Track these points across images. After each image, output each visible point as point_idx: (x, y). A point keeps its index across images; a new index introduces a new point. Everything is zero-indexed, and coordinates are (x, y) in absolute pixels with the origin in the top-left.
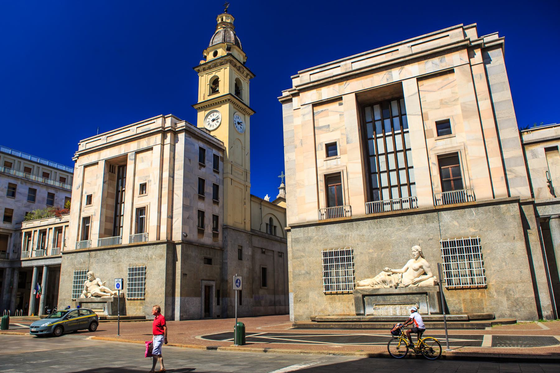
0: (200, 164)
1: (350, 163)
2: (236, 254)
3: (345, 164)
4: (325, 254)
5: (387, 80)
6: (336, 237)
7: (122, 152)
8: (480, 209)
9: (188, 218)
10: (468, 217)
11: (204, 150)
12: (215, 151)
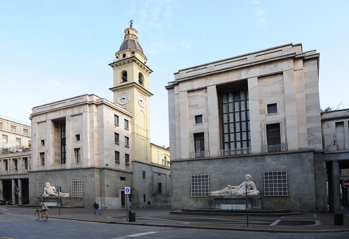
5: (238, 78)
7: (62, 116)
9: (108, 155)
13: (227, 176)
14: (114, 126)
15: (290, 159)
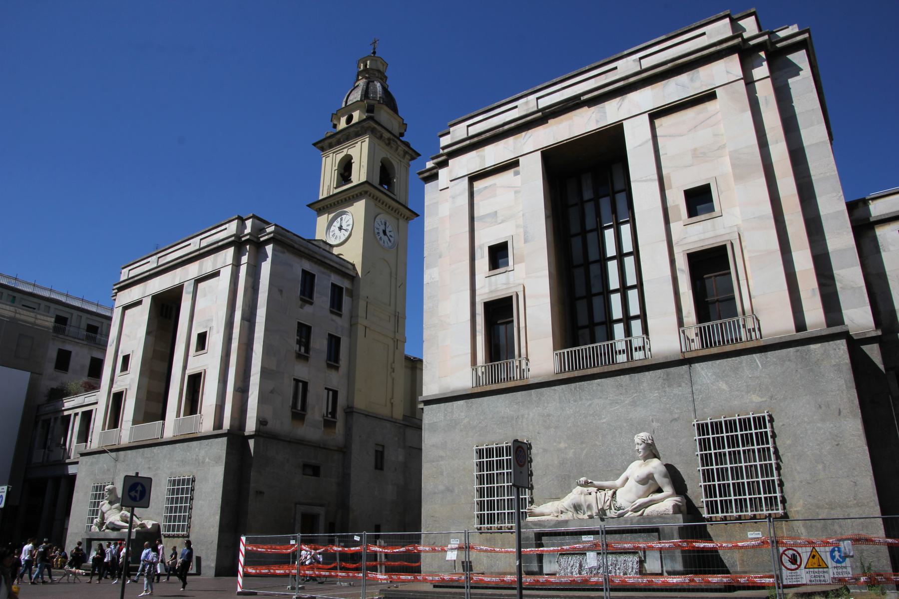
0: (301, 299)
2: (371, 459)
3: (521, 282)
4: (480, 453)
5: (597, 121)
7: (177, 282)
8: (770, 355)
9: (272, 392)
10: (747, 372)
11: (313, 276)
12: (335, 279)
13: (582, 443)
14: (300, 303)
15: (772, 367)
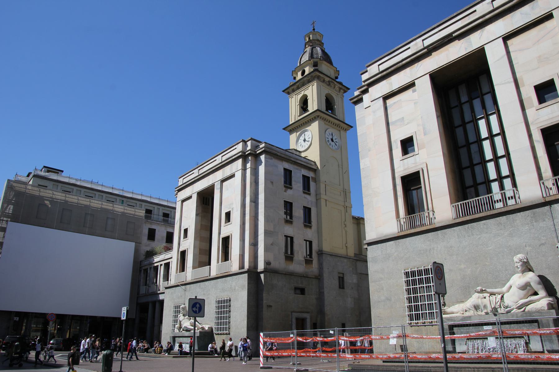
0: (285, 187)
1: (431, 160)
2: (336, 282)
4: (407, 274)
5: (466, 49)
6: (421, 252)
7: (211, 183)
9: (272, 244)
11: (291, 171)
12: (305, 172)
13: (476, 264)
14: (284, 188)
